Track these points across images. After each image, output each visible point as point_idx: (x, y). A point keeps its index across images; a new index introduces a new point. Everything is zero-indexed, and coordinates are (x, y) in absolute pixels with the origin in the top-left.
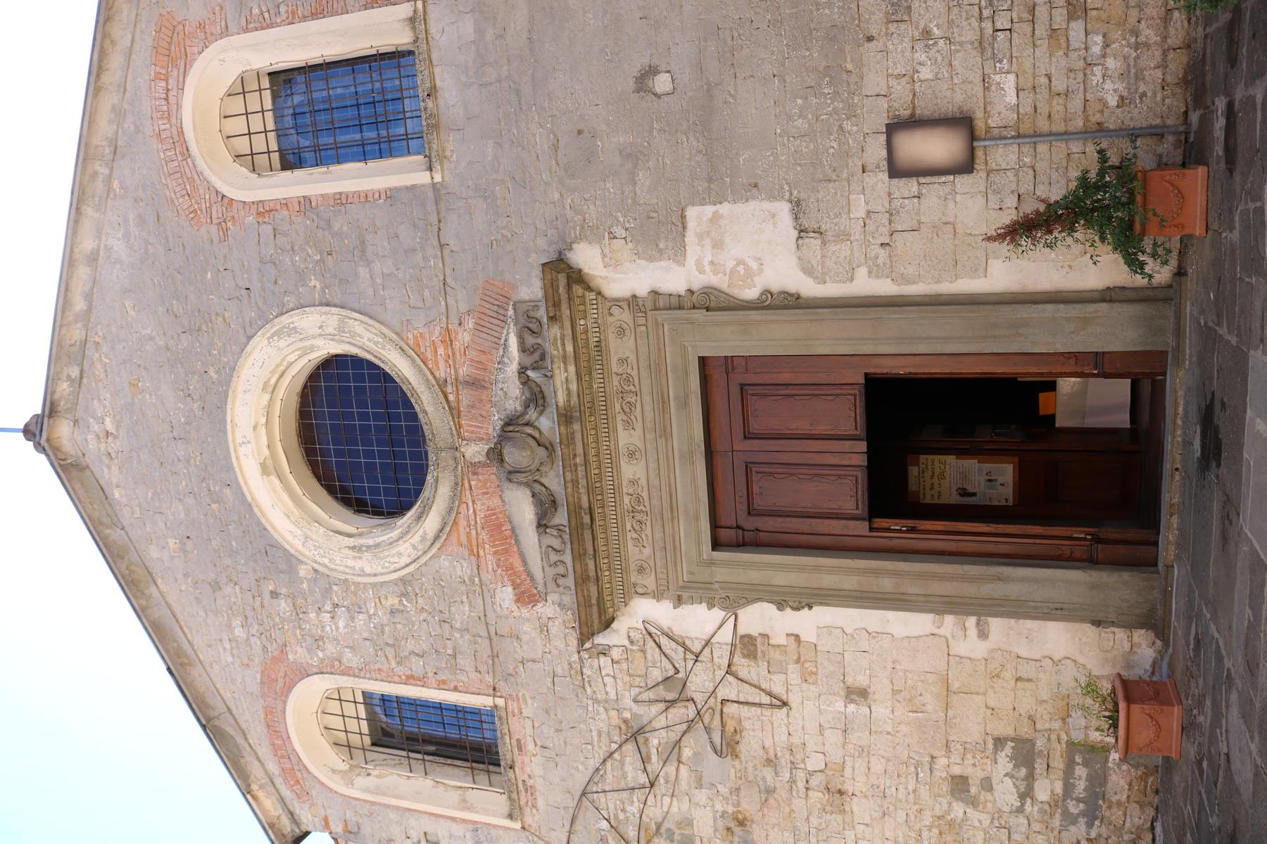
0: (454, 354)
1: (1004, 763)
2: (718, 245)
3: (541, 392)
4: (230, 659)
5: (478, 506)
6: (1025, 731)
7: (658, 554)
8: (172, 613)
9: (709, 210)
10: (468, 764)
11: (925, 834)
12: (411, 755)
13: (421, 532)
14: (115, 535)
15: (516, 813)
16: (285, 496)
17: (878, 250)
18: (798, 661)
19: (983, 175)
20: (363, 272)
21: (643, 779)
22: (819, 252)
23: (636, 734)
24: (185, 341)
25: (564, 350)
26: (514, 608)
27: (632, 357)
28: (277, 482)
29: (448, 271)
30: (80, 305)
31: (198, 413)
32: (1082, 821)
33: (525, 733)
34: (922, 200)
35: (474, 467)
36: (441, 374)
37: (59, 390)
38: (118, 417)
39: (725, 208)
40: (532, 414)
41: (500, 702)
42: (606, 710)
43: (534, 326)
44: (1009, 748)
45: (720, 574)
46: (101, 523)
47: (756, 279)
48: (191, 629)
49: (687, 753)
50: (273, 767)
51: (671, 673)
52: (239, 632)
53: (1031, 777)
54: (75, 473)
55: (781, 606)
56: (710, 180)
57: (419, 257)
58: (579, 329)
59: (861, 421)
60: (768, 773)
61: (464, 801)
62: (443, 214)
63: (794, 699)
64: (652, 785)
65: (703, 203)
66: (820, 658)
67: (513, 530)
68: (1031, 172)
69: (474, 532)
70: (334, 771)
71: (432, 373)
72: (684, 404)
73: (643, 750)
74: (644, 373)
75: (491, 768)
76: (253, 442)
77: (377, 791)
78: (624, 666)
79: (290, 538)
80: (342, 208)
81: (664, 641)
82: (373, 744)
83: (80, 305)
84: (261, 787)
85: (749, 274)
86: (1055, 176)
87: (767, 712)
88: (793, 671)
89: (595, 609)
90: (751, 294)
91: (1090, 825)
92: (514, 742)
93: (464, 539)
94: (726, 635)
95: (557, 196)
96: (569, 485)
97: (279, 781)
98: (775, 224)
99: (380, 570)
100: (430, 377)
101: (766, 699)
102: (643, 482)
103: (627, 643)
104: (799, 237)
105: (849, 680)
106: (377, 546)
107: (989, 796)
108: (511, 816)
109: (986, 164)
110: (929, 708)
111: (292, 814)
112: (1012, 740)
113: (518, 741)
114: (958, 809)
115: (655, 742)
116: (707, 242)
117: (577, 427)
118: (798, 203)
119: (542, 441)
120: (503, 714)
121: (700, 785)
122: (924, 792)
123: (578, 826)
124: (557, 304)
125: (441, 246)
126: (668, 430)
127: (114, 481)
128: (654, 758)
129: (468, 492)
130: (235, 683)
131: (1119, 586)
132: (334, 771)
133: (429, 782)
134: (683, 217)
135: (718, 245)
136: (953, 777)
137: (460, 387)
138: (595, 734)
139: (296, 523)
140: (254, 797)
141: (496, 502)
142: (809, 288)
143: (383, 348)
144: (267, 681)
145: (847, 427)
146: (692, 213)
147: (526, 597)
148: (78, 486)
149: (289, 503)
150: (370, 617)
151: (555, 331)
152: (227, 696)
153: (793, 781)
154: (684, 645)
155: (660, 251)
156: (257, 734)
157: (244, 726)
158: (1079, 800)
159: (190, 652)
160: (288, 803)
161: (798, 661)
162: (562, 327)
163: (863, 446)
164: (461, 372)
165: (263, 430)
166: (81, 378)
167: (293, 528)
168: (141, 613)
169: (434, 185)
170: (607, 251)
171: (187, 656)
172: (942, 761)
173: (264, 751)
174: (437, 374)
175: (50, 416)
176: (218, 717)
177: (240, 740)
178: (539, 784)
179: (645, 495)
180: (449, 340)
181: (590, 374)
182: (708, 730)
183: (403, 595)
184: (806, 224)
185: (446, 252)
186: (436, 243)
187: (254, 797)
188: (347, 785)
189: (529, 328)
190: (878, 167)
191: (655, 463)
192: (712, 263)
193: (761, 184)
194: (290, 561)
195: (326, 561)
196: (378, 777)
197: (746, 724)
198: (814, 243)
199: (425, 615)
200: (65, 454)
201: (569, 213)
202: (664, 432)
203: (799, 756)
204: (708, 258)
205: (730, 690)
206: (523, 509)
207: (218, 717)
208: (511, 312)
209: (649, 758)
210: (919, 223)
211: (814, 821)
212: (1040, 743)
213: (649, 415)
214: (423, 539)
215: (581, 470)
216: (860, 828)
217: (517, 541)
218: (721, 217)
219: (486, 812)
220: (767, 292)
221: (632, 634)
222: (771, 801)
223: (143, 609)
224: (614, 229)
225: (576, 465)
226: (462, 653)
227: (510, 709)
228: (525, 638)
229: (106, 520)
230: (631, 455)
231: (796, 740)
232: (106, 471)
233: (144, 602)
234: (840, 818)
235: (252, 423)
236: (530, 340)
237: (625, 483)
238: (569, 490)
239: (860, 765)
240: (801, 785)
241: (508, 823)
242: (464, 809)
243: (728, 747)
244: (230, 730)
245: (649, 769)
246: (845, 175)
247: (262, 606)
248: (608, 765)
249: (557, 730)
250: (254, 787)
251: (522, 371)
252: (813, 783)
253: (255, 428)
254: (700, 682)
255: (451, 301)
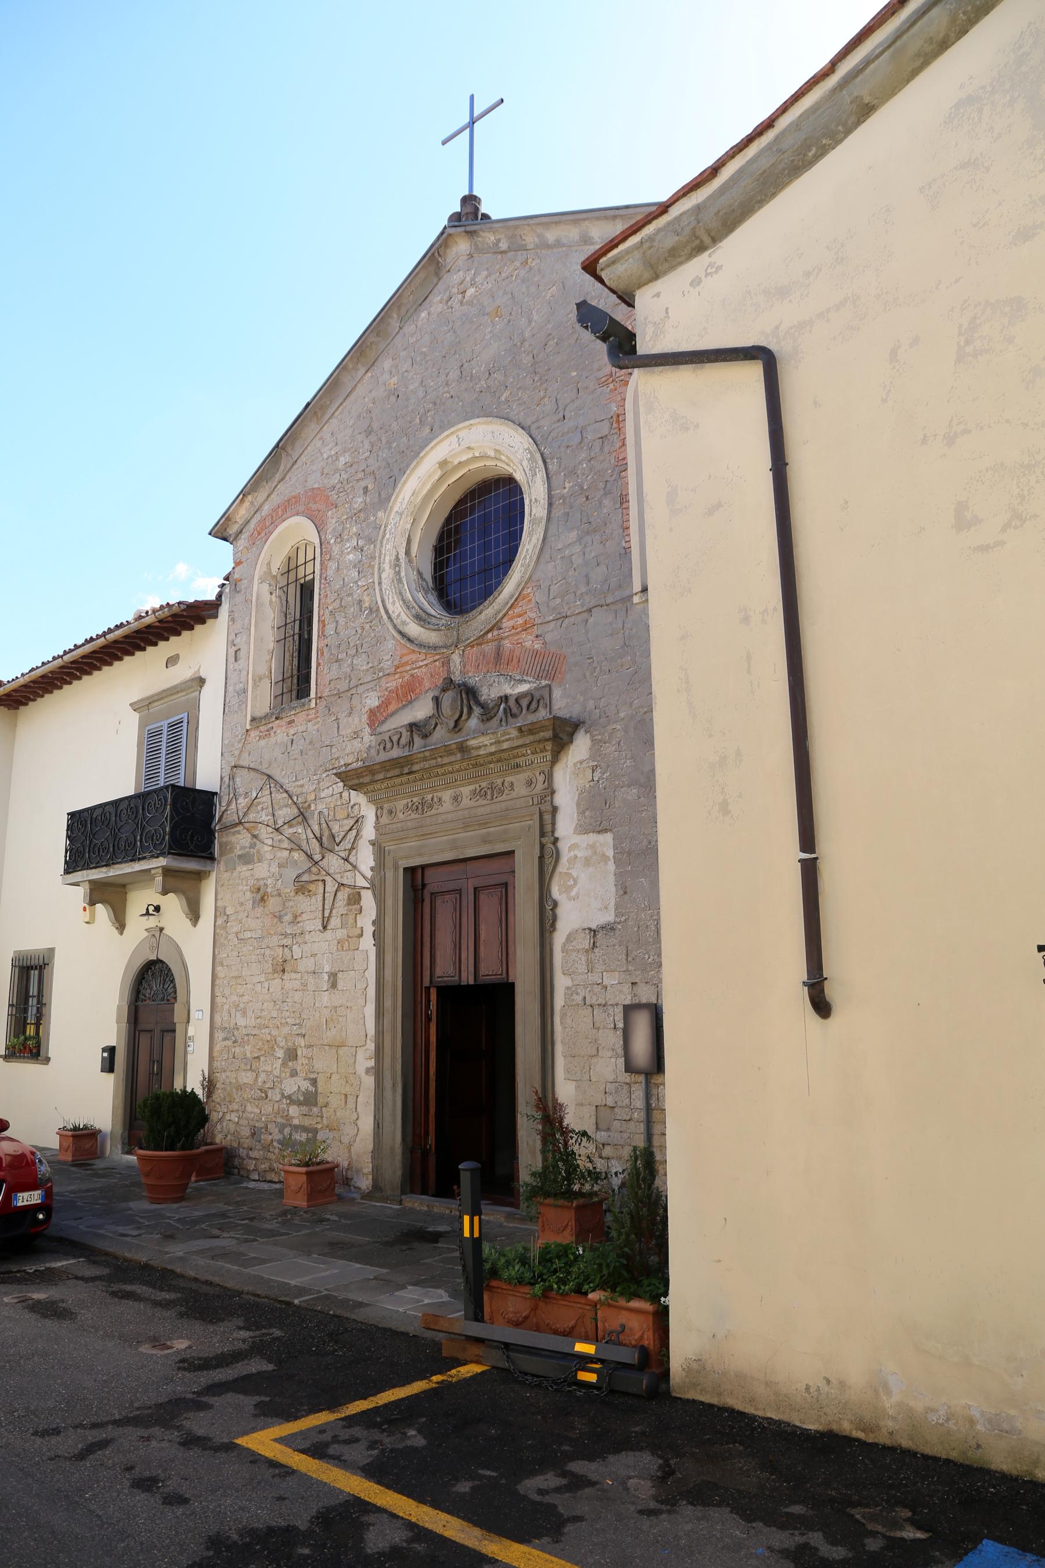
0: (518, 633)
1: (305, 1085)
2: (587, 862)
3: (492, 718)
4: (325, 456)
5: (424, 670)
6: (321, 1100)
7: (399, 825)
8: (350, 393)
9: (610, 853)
10: (295, 672)
11: (267, 1031)
12: (297, 623)
13: (408, 620)
14: (394, 323)
15: (255, 724)
16: (428, 487)
17: (582, 994)
18: (348, 937)
19: (628, 1080)
20: (574, 535)
21: (280, 823)
22: (581, 946)
23: (303, 816)
24: (527, 360)
25: (503, 741)
26: (367, 708)
27: (514, 794)
28: (437, 478)
29: (572, 620)
30: (551, 236)
31: (478, 388)
32: (281, 1137)
33: (305, 721)
34: (612, 1031)
35: (447, 663)
36: (507, 624)
37: (487, 234)
38: (475, 302)
39: (611, 866)
40: (477, 711)
41: (313, 704)
42: (315, 790)
43: (534, 705)
44: (312, 1089)
45: (389, 875)
46: (399, 308)
47: (564, 895)
48: (342, 413)
49: (295, 855)
50: (266, 509)
51: (338, 840)
52: (342, 460)
53: (300, 1104)
54: (432, 268)
55: (374, 923)
56: (629, 853)
57: (583, 589)
58: (523, 750)
59: (487, 980)
60: (288, 918)
61: (261, 679)
62: (613, 607)
63: (328, 934)
64: (277, 830)
65: (615, 848)
66: (351, 953)
67: (410, 702)
68: (628, 1118)
69: (408, 668)
70: (269, 564)
71: (505, 615)
72: (486, 840)
73: (294, 822)
74: (503, 805)
75: (294, 693)
76: (461, 447)
77: (259, 605)
78: (339, 803)
79: (400, 499)
80: (618, 505)
81: (354, 832)
82: (302, 585)
83: (551, 236)
84: (252, 503)
85: (568, 889)
86: (625, 1135)
87: (320, 916)
88: (341, 934)
89: (356, 781)
90: (556, 892)
91: (279, 1142)
92: (293, 717)
93: (405, 659)
94: (361, 882)
95: (622, 715)
96: (422, 755)
97: (258, 517)
98: (600, 910)
99: (384, 586)
100: (501, 615)
101: (327, 915)
102: (441, 810)
103: (352, 803)
104: (590, 929)
105: (340, 975)
106: (400, 581)
107: (288, 1074)
108: (253, 719)
109: (636, 1083)
110: (328, 1033)
111: (241, 532)
112: (316, 1091)
113: (293, 721)
114: (280, 1053)
115: (300, 831)
116: (589, 853)
117: (459, 756)
118: (612, 929)
119: (461, 723)
120: (306, 707)
121: (280, 866)
122: (286, 1030)
123: (253, 774)
124: (531, 732)
125: (590, 610)
126: (469, 829)
127: (432, 309)
128: (291, 830)
129: (432, 659)
130: (307, 473)
131: (394, 1170)
132: (269, 564)
133: (271, 645)
134: (606, 831)
135: (587, 862)
136: (296, 1050)
137: (496, 643)
138: (301, 782)
139: (410, 502)
140: (242, 500)
141: (427, 684)
142: (559, 939)
143: (522, 565)
144: (314, 494)
145: (483, 970)
146: (608, 837)
147: (375, 718)
148: (422, 275)
149: (424, 492)
150: (356, 582)
151: (514, 733)
152: (303, 459)
153: (286, 935)
154: (352, 848)
155: (583, 812)
156: (285, 490)
157: (287, 477)
158: (291, 1135)
159: (327, 417)
160: (247, 527)
161: (348, 937)
162: (517, 738)
163: (471, 982)
164: (506, 642)
165: (470, 456)
166: (502, 252)
167: (406, 502)
168: (342, 367)
169: (631, 596)
170: (585, 765)
171: (323, 415)
172: (302, 1042)
173: (276, 499)
174: (504, 620)
175: (466, 232)
176: (288, 454)
177: (278, 477)
178: (272, 740)
179: (433, 812)
180: (526, 627)
181: (498, 761)
182: (309, 870)
183: (371, 609)
184: (599, 936)
185: (585, 615)
186: (592, 605)
187: (242, 500)
188: (215, 616)
189: (533, 701)
190: (635, 995)
191: (452, 821)
192: (576, 857)
193: (627, 897)
194: (383, 501)
195: (387, 536)
196: (271, 601)
197: (313, 899)
198: (585, 943)
199: (359, 631)
200: (445, 253)
201: (610, 728)
202: (466, 827)
203: (299, 939)
204: (579, 855)
205: (331, 887)
206: (421, 710)
207: (288, 454)
208: (544, 683)
209: (291, 827)
210: (598, 1029)
211: (268, 952)
212: (315, 1109)
213: (480, 811)
214: (404, 623)
215: (433, 762)
216: (266, 985)
217: (404, 706)
218: (606, 864)
219: (254, 699)
220: (555, 904)
221: (357, 807)
222: (276, 920)
223: (345, 368)
224: (599, 771)
225: (435, 758)
226: (340, 666)
227: (311, 712)
228: (350, 719)
229: (403, 311)
230: (455, 799)
231: (307, 937)
232: (439, 298)
233: (350, 366)
234: (270, 970)
235: (472, 445)
236: (524, 703)
237: (439, 794)
238: (419, 755)
239: (297, 984)
240: (285, 942)
241: (249, 718)
242: (254, 680)
243: (302, 888)
244: (282, 468)
245: (286, 827)
246: (630, 968)
247: (358, 481)
248: (285, 795)
249: (302, 752)
250: (250, 498)
251: (505, 698)
252: (286, 949)
253: (469, 448)
254: (333, 863)
255: (552, 624)
